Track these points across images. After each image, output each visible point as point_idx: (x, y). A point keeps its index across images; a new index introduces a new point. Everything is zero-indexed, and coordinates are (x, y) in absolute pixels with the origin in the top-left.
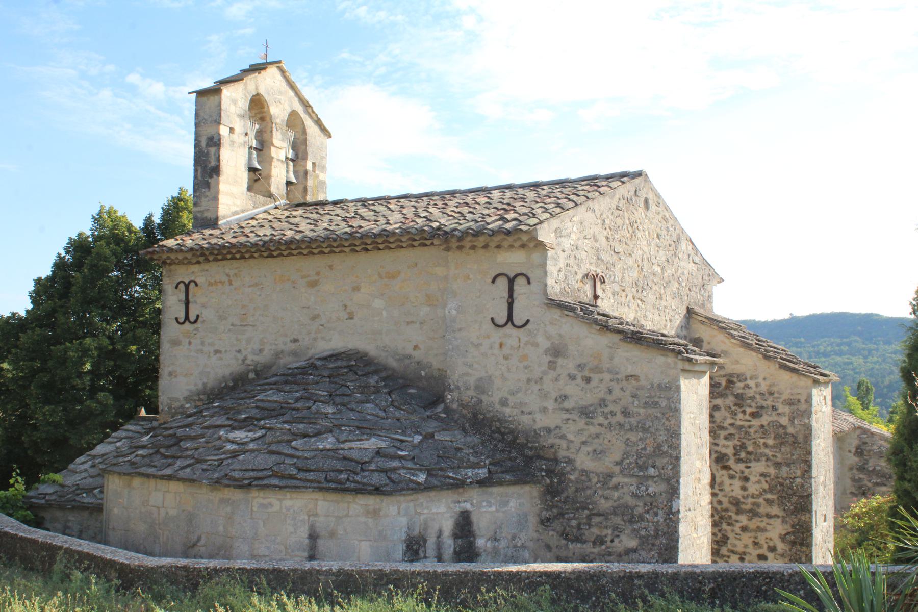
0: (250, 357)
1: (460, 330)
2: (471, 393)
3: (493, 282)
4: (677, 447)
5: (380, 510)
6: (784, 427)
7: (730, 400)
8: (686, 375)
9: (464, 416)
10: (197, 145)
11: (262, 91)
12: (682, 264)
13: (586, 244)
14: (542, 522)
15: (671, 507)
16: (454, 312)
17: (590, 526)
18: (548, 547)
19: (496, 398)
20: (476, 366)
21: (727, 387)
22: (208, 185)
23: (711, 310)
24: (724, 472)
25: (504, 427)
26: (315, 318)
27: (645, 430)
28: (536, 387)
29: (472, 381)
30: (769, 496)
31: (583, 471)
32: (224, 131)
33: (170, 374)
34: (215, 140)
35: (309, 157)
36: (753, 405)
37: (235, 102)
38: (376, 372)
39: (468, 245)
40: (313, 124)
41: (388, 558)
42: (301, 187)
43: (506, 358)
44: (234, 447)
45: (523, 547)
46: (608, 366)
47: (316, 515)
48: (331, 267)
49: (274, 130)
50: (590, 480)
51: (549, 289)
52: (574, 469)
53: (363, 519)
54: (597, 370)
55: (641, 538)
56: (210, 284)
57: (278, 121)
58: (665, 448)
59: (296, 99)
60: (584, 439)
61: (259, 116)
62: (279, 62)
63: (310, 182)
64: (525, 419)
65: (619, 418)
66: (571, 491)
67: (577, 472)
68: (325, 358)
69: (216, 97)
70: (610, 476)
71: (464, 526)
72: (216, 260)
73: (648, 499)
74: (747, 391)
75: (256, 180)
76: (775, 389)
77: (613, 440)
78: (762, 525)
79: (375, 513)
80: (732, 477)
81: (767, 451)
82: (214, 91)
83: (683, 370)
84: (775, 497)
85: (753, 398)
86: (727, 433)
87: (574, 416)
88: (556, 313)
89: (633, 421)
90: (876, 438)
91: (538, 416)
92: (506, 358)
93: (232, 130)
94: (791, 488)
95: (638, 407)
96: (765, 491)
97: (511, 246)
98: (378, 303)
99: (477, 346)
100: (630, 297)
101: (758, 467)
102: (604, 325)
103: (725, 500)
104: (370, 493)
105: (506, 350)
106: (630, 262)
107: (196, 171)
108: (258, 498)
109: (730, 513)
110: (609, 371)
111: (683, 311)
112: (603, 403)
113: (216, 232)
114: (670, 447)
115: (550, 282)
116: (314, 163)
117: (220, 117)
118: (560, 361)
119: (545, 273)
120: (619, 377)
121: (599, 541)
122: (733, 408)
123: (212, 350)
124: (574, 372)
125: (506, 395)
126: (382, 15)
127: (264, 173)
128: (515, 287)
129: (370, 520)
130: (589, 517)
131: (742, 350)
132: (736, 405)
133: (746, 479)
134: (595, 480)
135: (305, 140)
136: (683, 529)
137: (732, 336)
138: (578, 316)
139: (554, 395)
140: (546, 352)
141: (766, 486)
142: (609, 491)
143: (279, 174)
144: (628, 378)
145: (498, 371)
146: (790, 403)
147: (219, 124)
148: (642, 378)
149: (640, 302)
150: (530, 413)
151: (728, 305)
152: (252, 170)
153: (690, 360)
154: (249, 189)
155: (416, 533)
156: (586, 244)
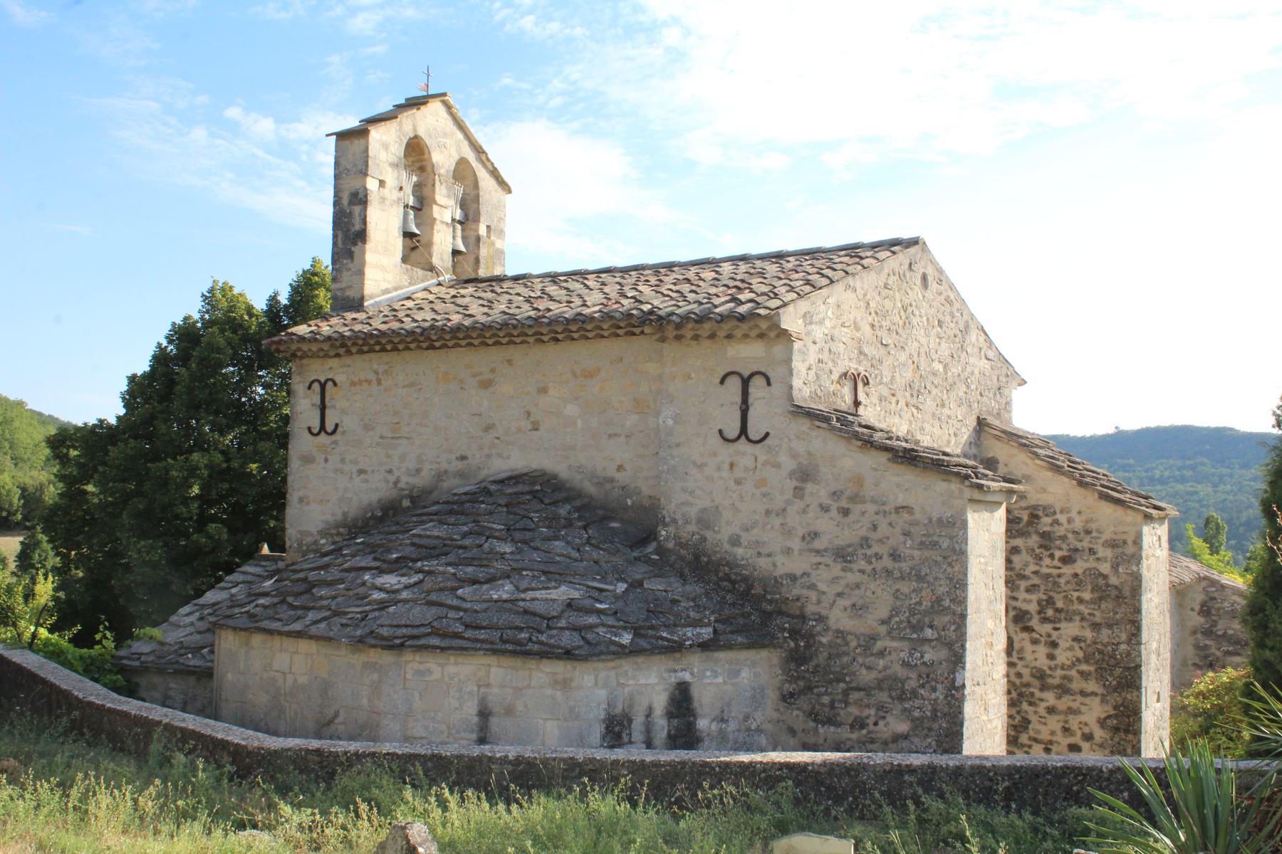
0: (404, 479)
1: (678, 445)
2: (692, 528)
3: (722, 382)
5: (571, 680)
6: (1105, 577)
7: (1034, 540)
8: (975, 506)
9: (682, 559)
10: (337, 203)
11: (422, 133)
15: (954, 680)
16: (670, 422)
18: (792, 731)
20: (698, 492)
21: (1030, 523)
22: (350, 255)
23: (1009, 421)
24: (1025, 635)
25: (736, 574)
26: (488, 428)
27: (920, 578)
28: (777, 522)
29: (693, 512)
30: (1084, 667)
31: (838, 631)
32: (372, 184)
33: (301, 500)
34: (361, 196)
36: (1064, 546)
37: (386, 147)
38: (567, 500)
39: (689, 334)
41: (581, 742)
42: (471, 258)
43: (738, 482)
45: (759, 730)
46: (872, 494)
48: (509, 362)
49: (437, 183)
50: (847, 644)
51: (795, 393)
52: (827, 630)
56: (353, 384)
58: (947, 603)
59: (466, 143)
60: (840, 589)
61: (418, 165)
62: (444, 95)
63: (483, 252)
64: (763, 563)
65: (887, 562)
66: (822, 658)
67: (830, 633)
68: (501, 482)
69: (362, 141)
70: (873, 638)
71: (682, 702)
72: (361, 352)
73: (924, 669)
74: (1056, 528)
75: (414, 249)
76: (1093, 526)
77: (879, 592)
78: (1075, 705)
79: (565, 684)
81: (1082, 608)
83: (971, 500)
84: (1092, 668)
85: (1063, 538)
87: (827, 559)
88: (804, 425)
89: (905, 566)
90: (1229, 592)
91: (780, 559)
92: (738, 482)
94: (1113, 656)
95: (911, 548)
96: (1078, 660)
97: (746, 336)
98: (571, 410)
99: (700, 467)
101: (1070, 629)
102: (868, 440)
103: (1026, 672)
105: (739, 473)
106: (903, 357)
108: (413, 663)
109: (1032, 690)
110: (873, 501)
112: (865, 542)
113: (361, 316)
114: (953, 601)
115: (797, 383)
116: (488, 227)
117: (367, 166)
118: (809, 487)
119: (791, 371)
120: (887, 508)
121: (859, 724)
122: (1038, 551)
123: (354, 469)
126: (554, 27)
127: (424, 240)
128: (751, 390)
129: (558, 693)
130: (845, 693)
131: (1050, 474)
132: (1041, 546)
133: (1054, 645)
134: (853, 644)
135: (478, 196)
136: (969, 709)
137: (1036, 454)
138: (833, 428)
139: (801, 532)
140: (791, 475)
141: (1080, 654)
142: (872, 658)
143: (444, 240)
144: (898, 509)
145: (727, 498)
146: (1113, 544)
147: (366, 175)
148: (917, 509)
149: (915, 411)
150: (769, 555)
151: (1033, 414)
152: (408, 235)
153: (980, 487)
154: (405, 260)
155: (618, 710)
156: (845, 334)
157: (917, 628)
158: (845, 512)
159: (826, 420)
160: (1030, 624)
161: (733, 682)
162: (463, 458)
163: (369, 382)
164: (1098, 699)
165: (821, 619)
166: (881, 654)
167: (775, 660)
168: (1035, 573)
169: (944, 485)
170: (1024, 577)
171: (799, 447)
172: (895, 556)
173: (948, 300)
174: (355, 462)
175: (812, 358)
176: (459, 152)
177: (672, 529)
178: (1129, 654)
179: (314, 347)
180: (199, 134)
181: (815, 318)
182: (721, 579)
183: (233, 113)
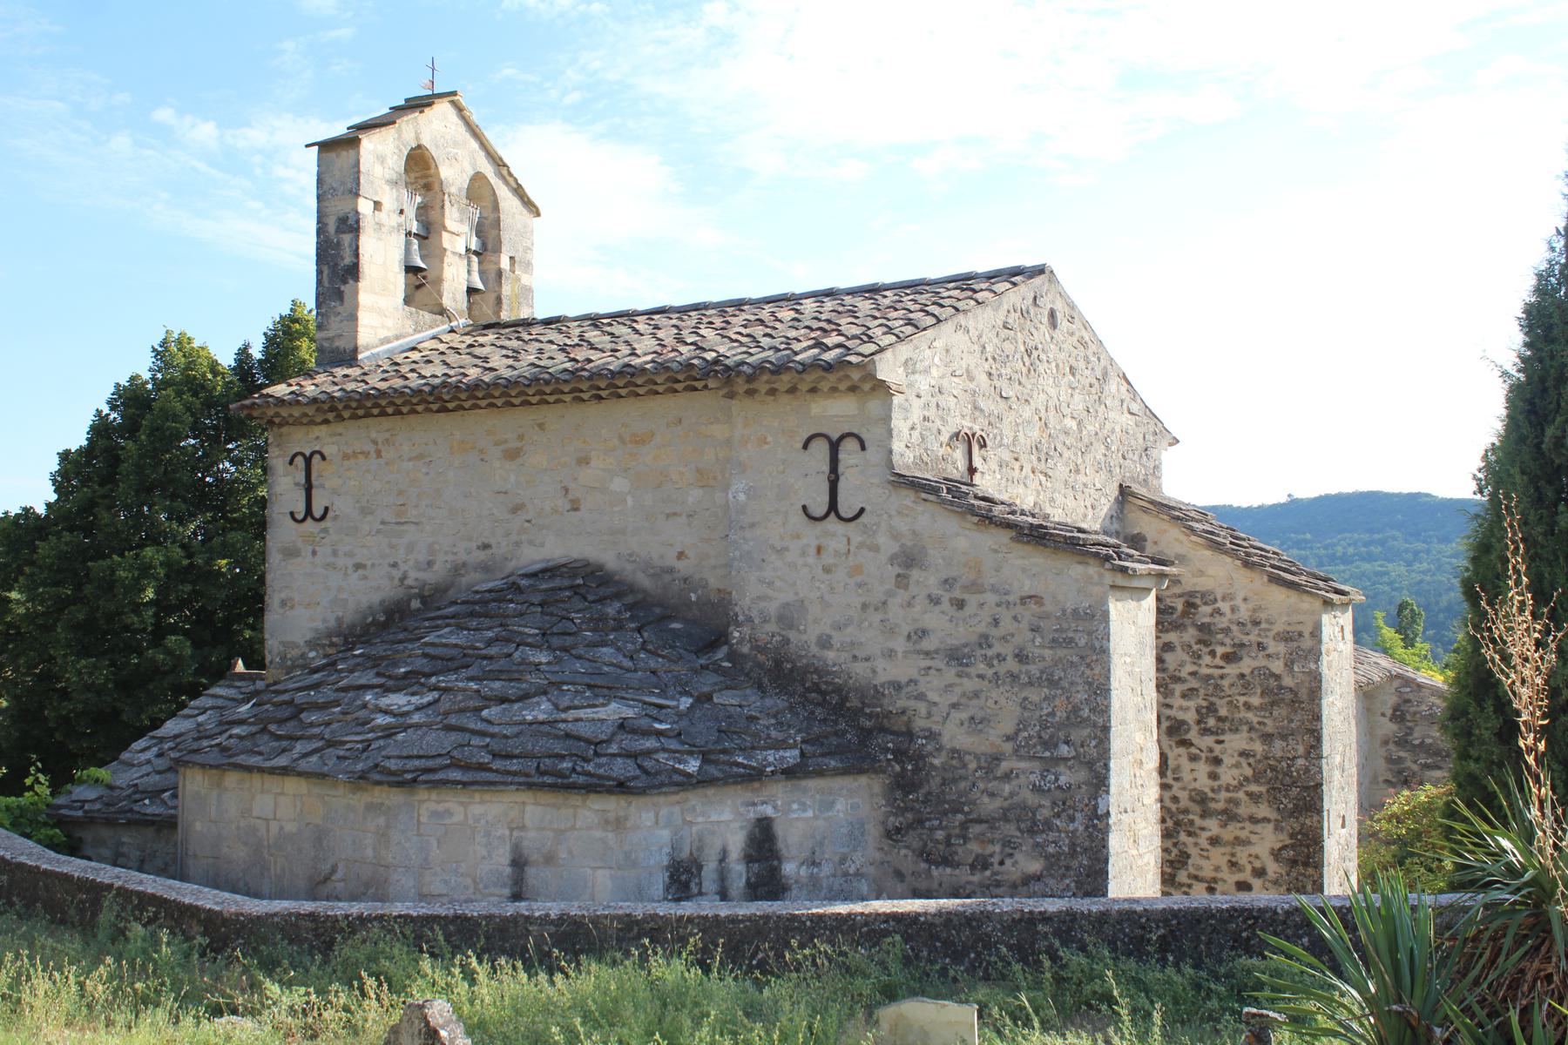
0: (413, 575)
1: (752, 525)
2: (772, 627)
3: (805, 447)
4: (1105, 711)
6: (1278, 677)
7: (1190, 634)
8: (1118, 594)
11: (426, 142)
12: (1112, 415)
13: (955, 385)
14: (888, 834)
15: (1096, 807)
16: (742, 497)
17: (966, 839)
18: (899, 875)
19: (811, 636)
20: (778, 583)
21: (1185, 614)
24: (1182, 750)
25: (826, 683)
26: (516, 509)
27: (1053, 684)
28: (876, 618)
29: (772, 608)
30: (1254, 788)
31: (954, 751)
32: (364, 207)
33: (283, 603)
34: (351, 222)
35: (504, 249)
36: (1228, 641)
37: (382, 159)
39: (764, 388)
40: (510, 195)
41: (640, 895)
42: (492, 297)
43: (827, 570)
44: (389, 719)
46: (992, 581)
47: (523, 828)
48: (541, 426)
49: (447, 204)
50: (965, 766)
51: (895, 458)
52: (939, 749)
53: (598, 834)
54: (975, 587)
55: (1047, 857)
56: (346, 457)
57: (453, 190)
58: (1085, 713)
59: (482, 154)
60: (955, 700)
61: (422, 182)
62: (454, 93)
63: (506, 290)
64: (860, 669)
66: (934, 784)
67: (944, 753)
68: (534, 575)
69: (352, 152)
70: (997, 758)
71: (763, 842)
72: (354, 417)
73: (1059, 795)
74: (1217, 619)
76: (1262, 616)
77: (1002, 701)
78: (1243, 834)
79: (619, 824)
80: (1193, 758)
81: (1250, 716)
82: (349, 142)
84: (1263, 789)
85: (1226, 631)
86: (1185, 687)
87: (939, 663)
88: (908, 498)
89: (1034, 669)
90: (1426, 692)
91: (880, 664)
92: (827, 570)
93: (377, 205)
95: (1042, 646)
96: (1247, 779)
97: (834, 389)
98: (619, 484)
99: (781, 551)
100: (1027, 469)
101: (1236, 742)
102: (986, 515)
104: (609, 791)
105: (827, 559)
106: (1027, 412)
107: (319, 273)
109: (1191, 817)
110: (994, 589)
111: (1113, 492)
113: (354, 372)
115: (897, 446)
116: (512, 258)
117: (358, 184)
118: (915, 574)
120: (1011, 598)
121: (981, 863)
122: (1195, 647)
123: (350, 562)
124: (937, 592)
125: (828, 631)
127: (431, 275)
128: (841, 456)
129: (610, 835)
130: (964, 826)
131: (1208, 553)
132: (1199, 642)
136: (1114, 842)
138: (943, 501)
140: (892, 560)
141: (1249, 772)
142: (995, 783)
143: (456, 276)
145: (807, 588)
146: (1286, 637)
147: (357, 195)
149: (1043, 478)
150: (867, 659)
151: (1188, 480)
152: (411, 270)
153: (1124, 570)
155: (685, 854)
156: (955, 385)
157: (1050, 744)
158: (960, 604)
159: (935, 491)
160: (1188, 736)
161: (826, 815)
162: (486, 546)
163: (366, 454)
164: (1271, 826)
165: (932, 736)
166: (1007, 777)
167: (877, 788)
168: (1193, 674)
169: (1080, 569)
170: (1178, 680)
171: (902, 525)
172: (1021, 657)
173: (1082, 342)
174: (350, 554)
175: (916, 415)
176: (474, 165)
177: (746, 630)
178: (1307, 770)
179: (296, 412)
180: (121, 142)
181: (919, 366)
182: (809, 690)
183: (164, 115)
